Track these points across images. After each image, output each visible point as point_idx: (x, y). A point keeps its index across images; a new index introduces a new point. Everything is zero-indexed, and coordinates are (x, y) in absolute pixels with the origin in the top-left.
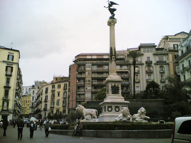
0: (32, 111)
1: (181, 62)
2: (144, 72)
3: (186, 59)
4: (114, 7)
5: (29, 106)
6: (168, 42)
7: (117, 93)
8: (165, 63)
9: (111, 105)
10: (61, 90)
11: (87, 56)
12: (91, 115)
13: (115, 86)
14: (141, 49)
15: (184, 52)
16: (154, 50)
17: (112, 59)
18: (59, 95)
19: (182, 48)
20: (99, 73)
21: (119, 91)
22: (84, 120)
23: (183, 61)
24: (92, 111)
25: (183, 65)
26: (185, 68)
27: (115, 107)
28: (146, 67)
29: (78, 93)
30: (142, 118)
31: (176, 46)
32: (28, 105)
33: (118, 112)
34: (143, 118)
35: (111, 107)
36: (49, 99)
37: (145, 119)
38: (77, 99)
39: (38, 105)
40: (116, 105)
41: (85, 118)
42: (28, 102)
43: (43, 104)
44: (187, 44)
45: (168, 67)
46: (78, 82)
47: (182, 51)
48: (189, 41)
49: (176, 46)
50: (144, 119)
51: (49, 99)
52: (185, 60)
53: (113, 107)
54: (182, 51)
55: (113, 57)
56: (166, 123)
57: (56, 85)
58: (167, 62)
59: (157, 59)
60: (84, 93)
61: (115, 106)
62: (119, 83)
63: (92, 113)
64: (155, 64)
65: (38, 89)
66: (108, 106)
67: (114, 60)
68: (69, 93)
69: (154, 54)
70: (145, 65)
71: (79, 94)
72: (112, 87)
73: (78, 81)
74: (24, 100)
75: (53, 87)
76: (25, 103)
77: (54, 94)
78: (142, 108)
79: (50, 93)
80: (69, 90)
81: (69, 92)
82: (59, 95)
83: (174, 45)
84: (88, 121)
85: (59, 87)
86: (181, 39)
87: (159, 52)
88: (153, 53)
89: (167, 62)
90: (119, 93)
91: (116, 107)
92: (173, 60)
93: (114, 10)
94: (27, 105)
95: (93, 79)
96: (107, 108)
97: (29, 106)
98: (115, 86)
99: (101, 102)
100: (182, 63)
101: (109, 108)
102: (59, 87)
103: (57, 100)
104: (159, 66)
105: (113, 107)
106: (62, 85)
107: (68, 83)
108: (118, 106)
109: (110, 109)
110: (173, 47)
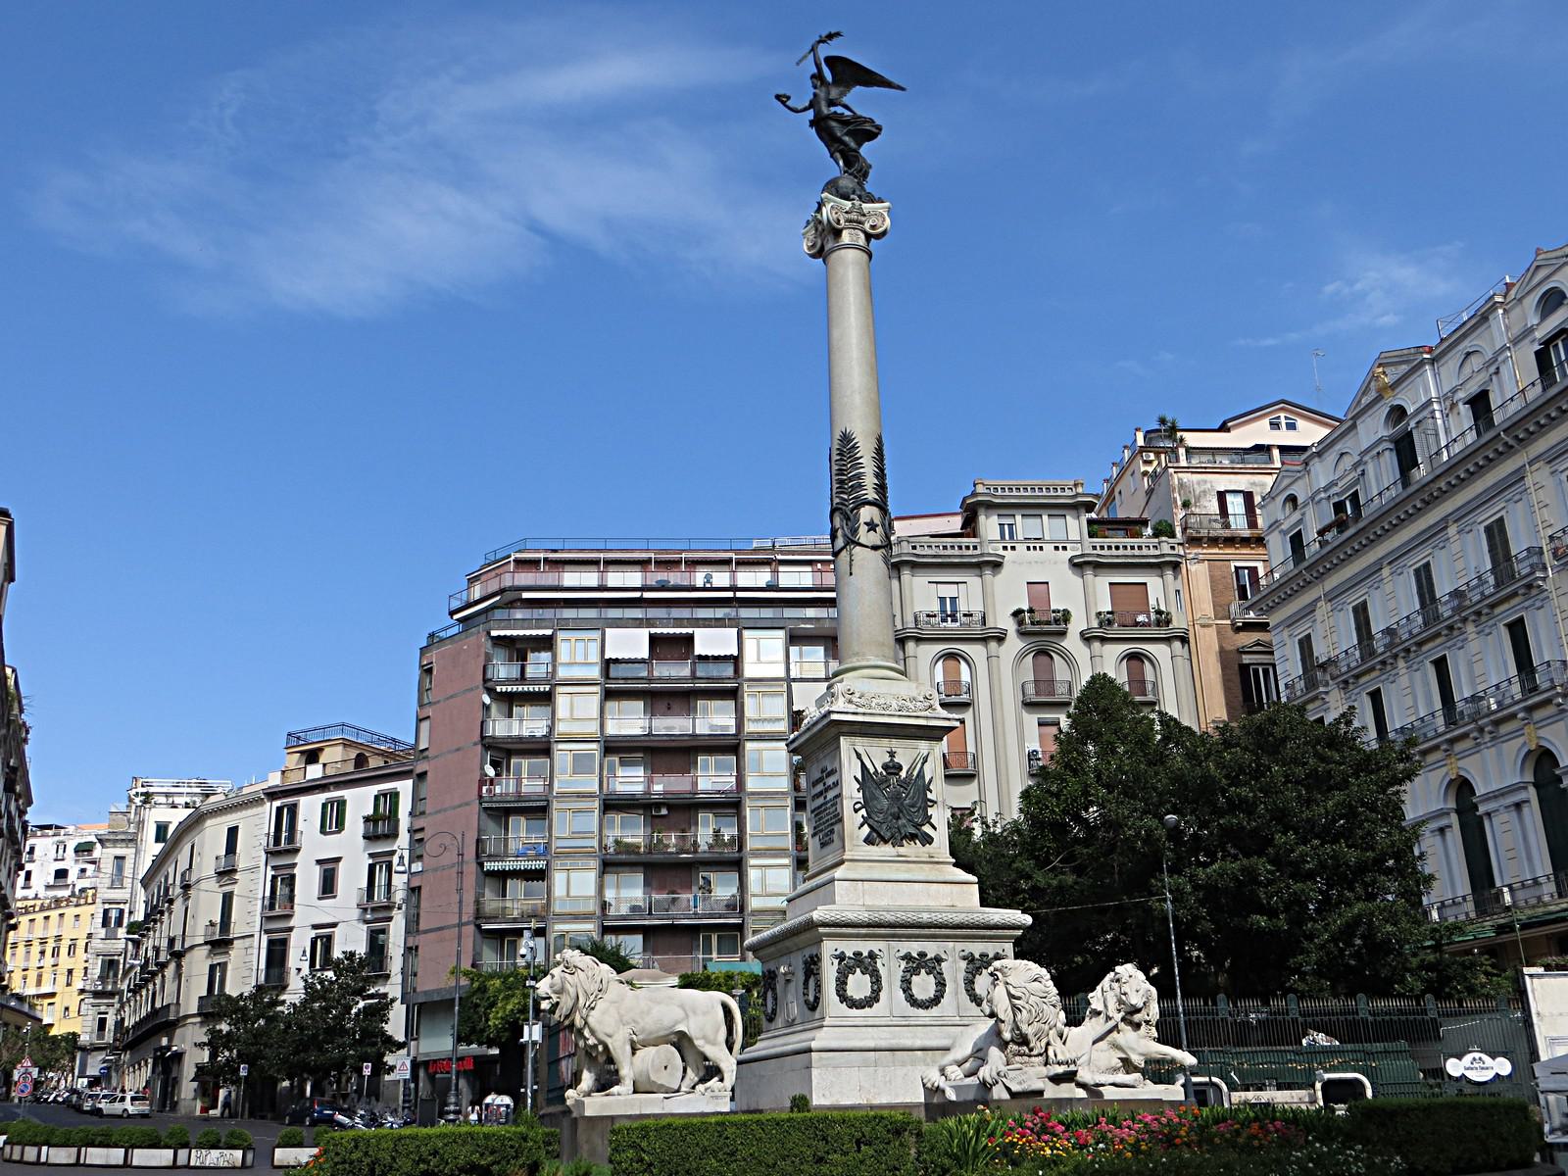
0: (102, 1023)
1: (1290, 623)
2: (1010, 699)
3: (1332, 597)
4: (859, 101)
5: (78, 984)
6: (1179, 469)
7: (912, 837)
8: (1162, 633)
9: (865, 947)
10: (351, 848)
11: (567, 568)
12: (681, 1042)
13: (893, 768)
14: (982, 518)
15: (1312, 550)
16: (1075, 527)
17: (855, 531)
18: (328, 887)
19: (1297, 516)
20: (660, 699)
21: (928, 819)
22: (620, 1102)
23: (1310, 610)
24: (687, 1011)
25: (1306, 644)
26: (1323, 667)
27: (963, 964)
28: (1022, 656)
29: (488, 866)
30: (1127, 1065)
31: (1236, 505)
32: (70, 972)
33: (935, 1011)
34: (1138, 1060)
35: (866, 964)
36: (247, 917)
37: (1159, 1071)
38: (479, 916)
39: (149, 974)
40: (914, 948)
41: (626, 1072)
42: (64, 951)
43: (198, 964)
44: (1333, 484)
45: (1182, 664)
46: (491, 772)
47: (1297, 541)
48: (1347, 462)
49: (1236, 505)
50: (1144, 1072)
51: (247, 917)
52: (1323, 608)
53: (891, 970)
54: (1297, 541)
55: (867, 513)
56: (1238, 1097)
57: (310, 807)
58: (1179, 622)
59: (1101, 591)
60: (541, 864)
61: (908, 957)
62: (923, 746)
63: (690, 1027)
64: (1087, 638)
65: (161, 845)
66: (841, 957)
67: (875, 548)
68: (417, 867)
69: (1078, 566)
70: (1014, 644)
71: (502, 876)
72: (867, 780)
73: (495, 764)
74: (39, 933)
75: (286, 823)
76: (48, 960)
77: (290, 881)
78: (1127, 970)
79: (254, 869)
80: (417, 842)
81: (415, 857)
82: (328, 887)
83: (1222, 496)
84: (653, 1105)
85: (334, 819)
86: (1276, 452)
87: (1118, 545)
88: (1070, 553)
89: (1179, 622)
90: (927, 840)
91: (916, 964)
92: (1221, 610)
93: (867, 132)
94: (62, 979)
95: (616, 748)
96: (829, 971)
97: (78, 984)
98: (893, 768)
99: (371, 1005)
100: (1301, 631)
101: (916, 971)
102: (334, 819)
103: (315, 927)
104: (1121, 648)
105: (891, 970)
106: (360, 801)
107: (405, 787)
108: (931, 949)
109: (859, 985)
110: (1213, 507)
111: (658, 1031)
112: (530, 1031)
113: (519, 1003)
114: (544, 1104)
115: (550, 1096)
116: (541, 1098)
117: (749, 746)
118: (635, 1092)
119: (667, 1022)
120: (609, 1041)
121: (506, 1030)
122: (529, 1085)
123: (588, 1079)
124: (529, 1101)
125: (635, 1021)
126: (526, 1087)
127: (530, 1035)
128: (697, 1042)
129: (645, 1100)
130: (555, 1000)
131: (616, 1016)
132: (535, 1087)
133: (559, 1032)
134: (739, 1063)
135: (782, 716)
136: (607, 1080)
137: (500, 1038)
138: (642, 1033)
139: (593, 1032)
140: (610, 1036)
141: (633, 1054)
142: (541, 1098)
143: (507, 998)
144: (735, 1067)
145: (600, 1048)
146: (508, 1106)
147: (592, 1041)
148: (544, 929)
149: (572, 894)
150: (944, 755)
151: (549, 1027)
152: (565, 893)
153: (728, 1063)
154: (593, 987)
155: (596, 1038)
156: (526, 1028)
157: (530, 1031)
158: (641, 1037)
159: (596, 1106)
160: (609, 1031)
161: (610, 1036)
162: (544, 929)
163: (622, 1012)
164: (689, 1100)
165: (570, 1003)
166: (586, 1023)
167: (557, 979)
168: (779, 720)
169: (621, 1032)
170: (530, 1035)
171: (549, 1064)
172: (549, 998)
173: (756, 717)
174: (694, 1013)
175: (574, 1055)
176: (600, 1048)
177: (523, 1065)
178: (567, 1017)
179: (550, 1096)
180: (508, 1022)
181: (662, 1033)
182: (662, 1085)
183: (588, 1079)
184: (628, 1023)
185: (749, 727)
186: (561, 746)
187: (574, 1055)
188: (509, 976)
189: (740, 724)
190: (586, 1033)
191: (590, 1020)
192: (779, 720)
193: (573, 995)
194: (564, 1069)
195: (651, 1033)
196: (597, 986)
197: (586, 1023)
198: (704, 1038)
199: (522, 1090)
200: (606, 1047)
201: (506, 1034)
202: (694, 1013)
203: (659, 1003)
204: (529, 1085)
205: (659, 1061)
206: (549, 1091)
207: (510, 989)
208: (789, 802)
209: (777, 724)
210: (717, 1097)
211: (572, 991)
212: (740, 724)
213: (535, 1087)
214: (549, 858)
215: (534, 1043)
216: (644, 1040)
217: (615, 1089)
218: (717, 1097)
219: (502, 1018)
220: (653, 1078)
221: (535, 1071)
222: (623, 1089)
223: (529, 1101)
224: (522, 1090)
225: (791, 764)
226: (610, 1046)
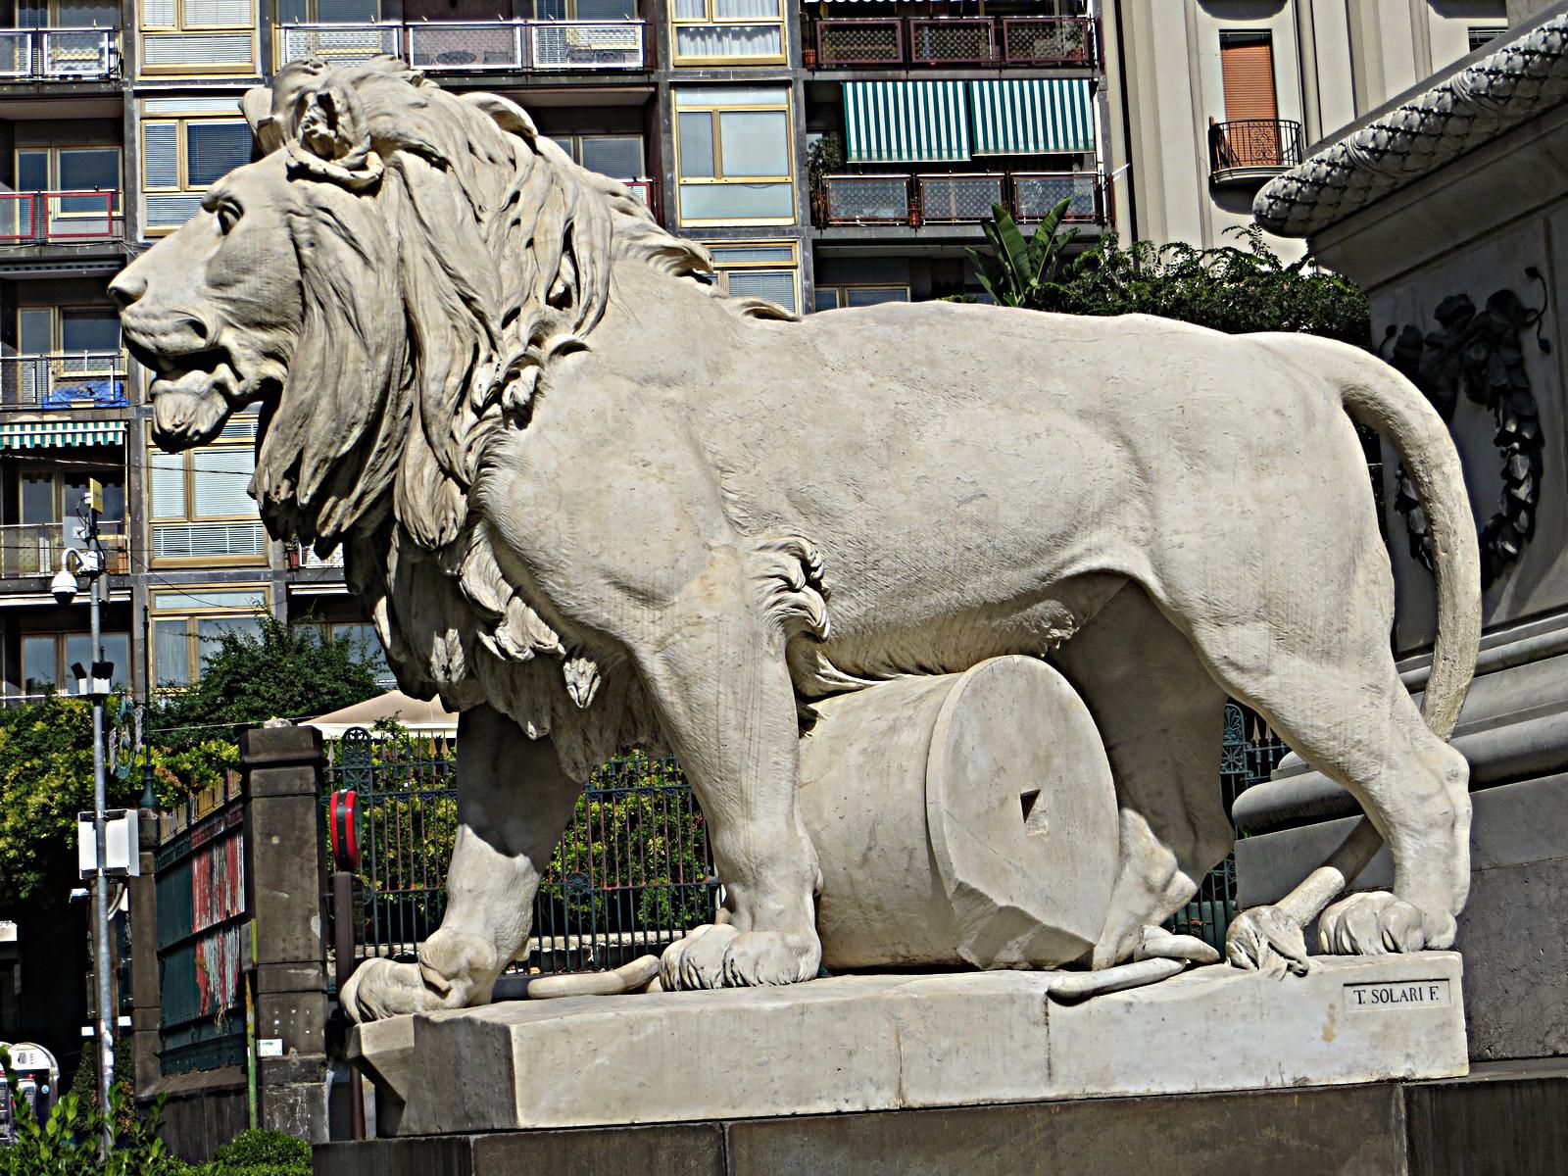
12: (1114, 639)
41: (771, 827)
84: (970, 1043)
111: (950, 576)
112: (100, 838)
113: (64, 787)
114: (153, 1065)
115: (171, 1045)
116: (143, 1052)
117: (682, 101)
118: (829, 968)
119: (1019, 508)
120: (639, 628)
121: (31, 866)
122: (106, 1011)
123: (487, 892)
124: (108, 1058)
125: (805, 506)
126: (94, 1023)
127: (101, 852)
128: (1214, 642)
129: (924, 1007)
130: (254, 370)
131: (689, 468)
132: (124, 1021)
133: (186, 861)
134: (1482, 776)
135: (771, 18)
136: (636, 867)
137: (15, 887)
138: (856, 579)
139: (523, 573)
140: (647, 597)
141: (806, 722)
142: (143, 1052)
143: (29, 777)
144: (1461, 798)
145: (581, 678)
146: (41, 1076)
147: (519, 633)
148: (127, 607)
149: (201, 511)
150: (1215, 132)
151: (158, 849)
152: (179, 511)
153: (1423, 785)
154: (513, 277)
155: (552, 614)
156: (85, 830)
157: (100, 838)
158: (848, 609)
159: (582, 1055)
160: (644, 564)
161: (647, 597)
162: (127, 607)
163: (721, 446)
164: (1209, 1004)
165: (363, 379)
166: (477, 512)
167: (259, 223)
168: (764, 30)
169: (722, 568)
170: (101, 852)
171: (163, 954)
172: (213, 356)
173: (701, 22)
174: (1195, 455)
175: (242, 919)
176: (581, 678)
177: (87, 964)
178: (341, 474)
179: (171, 1045)
180: (33, 843)
181: (983, 587)
182: (1019, 919)
183: (487, 892)
184: (768, 518)
185: (683, 52)
186: (153, 106)
187: (242, 919)
188: (31, 719)
189: (654, 47)
190: (481, 577)
191: (499, 488)
192: (764, 30)
193: (384, 323)
194: (212, 967)
195: (916, 584)
196: (545, 267)
197: (477, 512)
198: (1269, 610)
199: (87, 1031)
200: (622, 671)
201: (32, 877)
202: (1195, 455)
203: (958, 393)
204: (106, 1011)
205: (988, 757)
206: (166, 1033)
207: (36, 752)
208: (800, 255)
209: (758, 40)
210: (1383, 989)
211: (372, 290)
212: (654, 47)
213: (124, 1021)
214: (131, 413)
215: (117, 876)
216: (864, 632)
217: (701, 946)
218: (1383, 989)
219: (16, 832)
220: (962, 870)
221: (122, 977)
222: (760, 942)
223: (108, 1058)
224: (87, 1031)
225: (801, 154)
226: (654, 665)
